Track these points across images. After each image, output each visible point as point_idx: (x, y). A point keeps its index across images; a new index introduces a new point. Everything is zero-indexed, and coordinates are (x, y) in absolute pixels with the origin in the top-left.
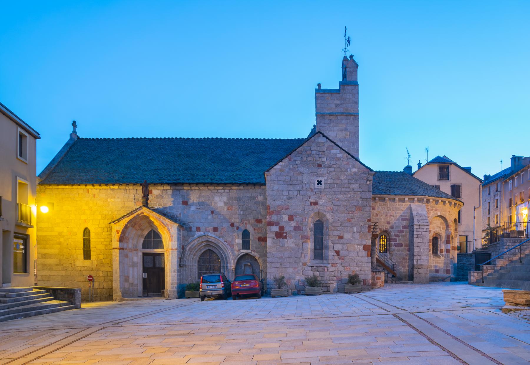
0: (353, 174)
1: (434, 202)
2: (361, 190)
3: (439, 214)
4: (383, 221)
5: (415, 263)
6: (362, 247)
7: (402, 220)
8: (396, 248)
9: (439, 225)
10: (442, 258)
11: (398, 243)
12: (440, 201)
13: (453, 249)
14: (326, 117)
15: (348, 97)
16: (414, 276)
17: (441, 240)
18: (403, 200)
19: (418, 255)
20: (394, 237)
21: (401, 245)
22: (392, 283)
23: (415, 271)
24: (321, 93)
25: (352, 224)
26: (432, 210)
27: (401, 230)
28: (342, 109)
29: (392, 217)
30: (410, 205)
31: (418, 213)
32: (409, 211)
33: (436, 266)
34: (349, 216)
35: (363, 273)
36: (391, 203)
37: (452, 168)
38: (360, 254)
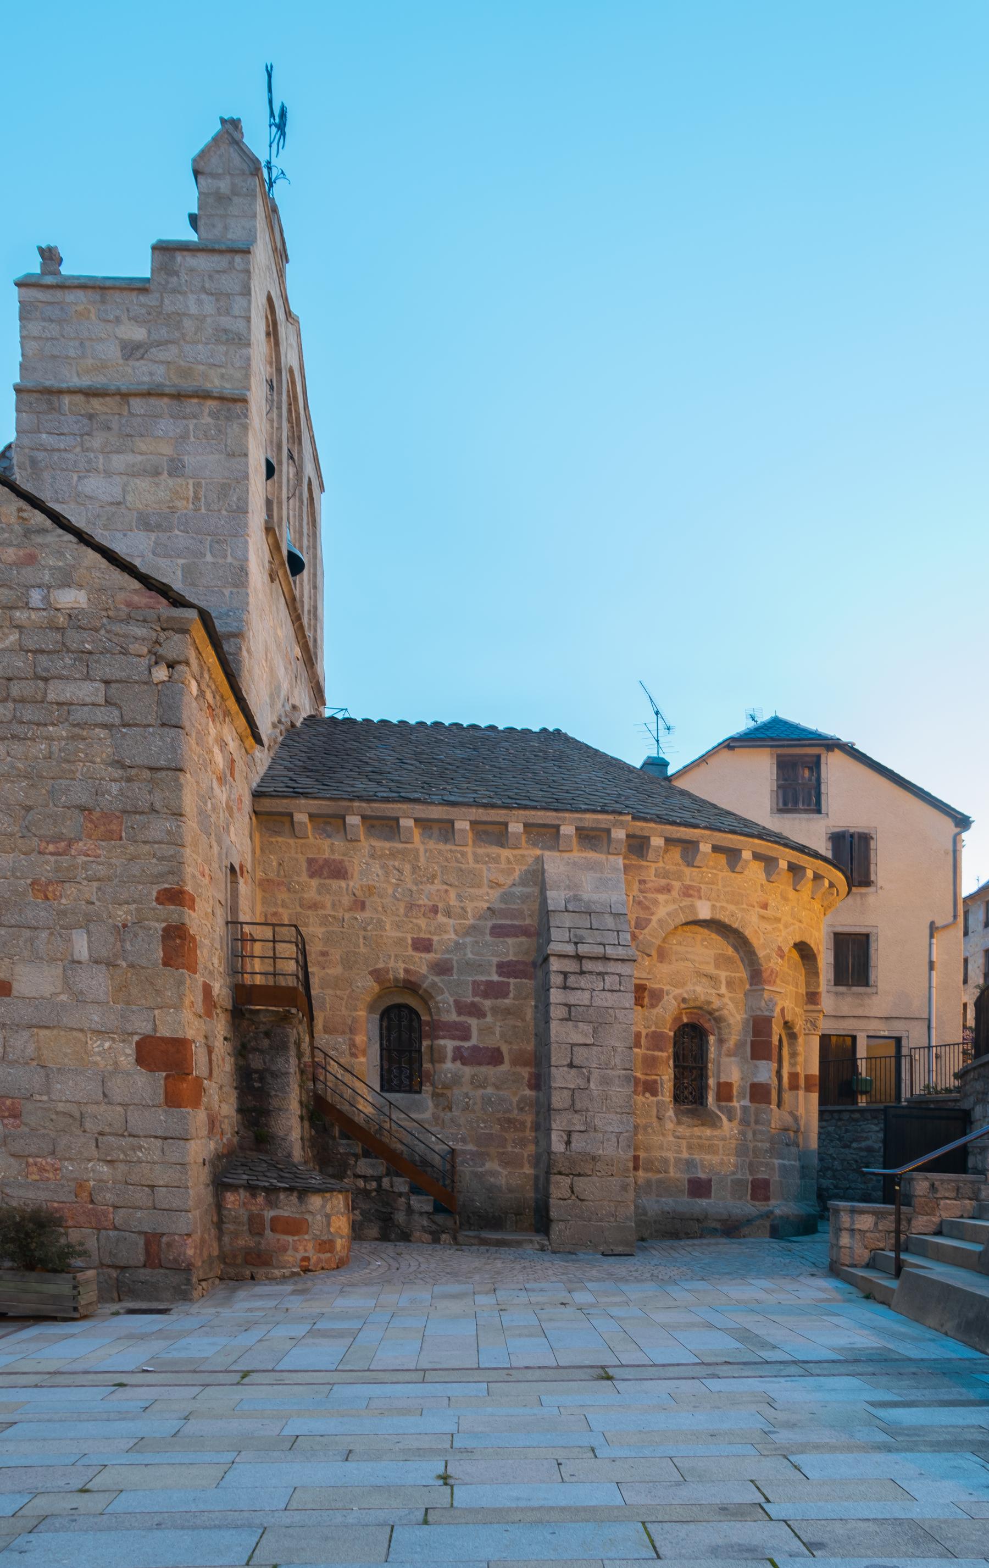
0: (61, 620)
1: (676, 854)
2: (113, 716)
3: (704, 912)
4: (391, 933)
5: (557, 1145)
6: (130, 1050)
7: (498, 931)
8: (468, 1071)
9: (711, 969)
10: (729, 1128)
11: (475, 1049)
12: (705, 848)
13: (794, 1087)
14: (66, 400)
15: (193, 310)
16: (553, 1214)
17: (721, 1041)
18: (495, 834)
19: (573, 1108)
20: (454, 1017)
21: (495, 1057)
22: (436, 1240)
23: (559, 1187)
24: (47, 287)
25: (62, 913)
26: (667, 889)
27: (489, 984)
28: (161, 370)
29: (441, 918)
30: (539, 860)
31: (577, 898)
32: (535, 890)
33: (690, 1164)
34: (46, 867)
35: (141, 1196)
36: (431, 845)
37: (833, 765)
38: (118, 1089)
